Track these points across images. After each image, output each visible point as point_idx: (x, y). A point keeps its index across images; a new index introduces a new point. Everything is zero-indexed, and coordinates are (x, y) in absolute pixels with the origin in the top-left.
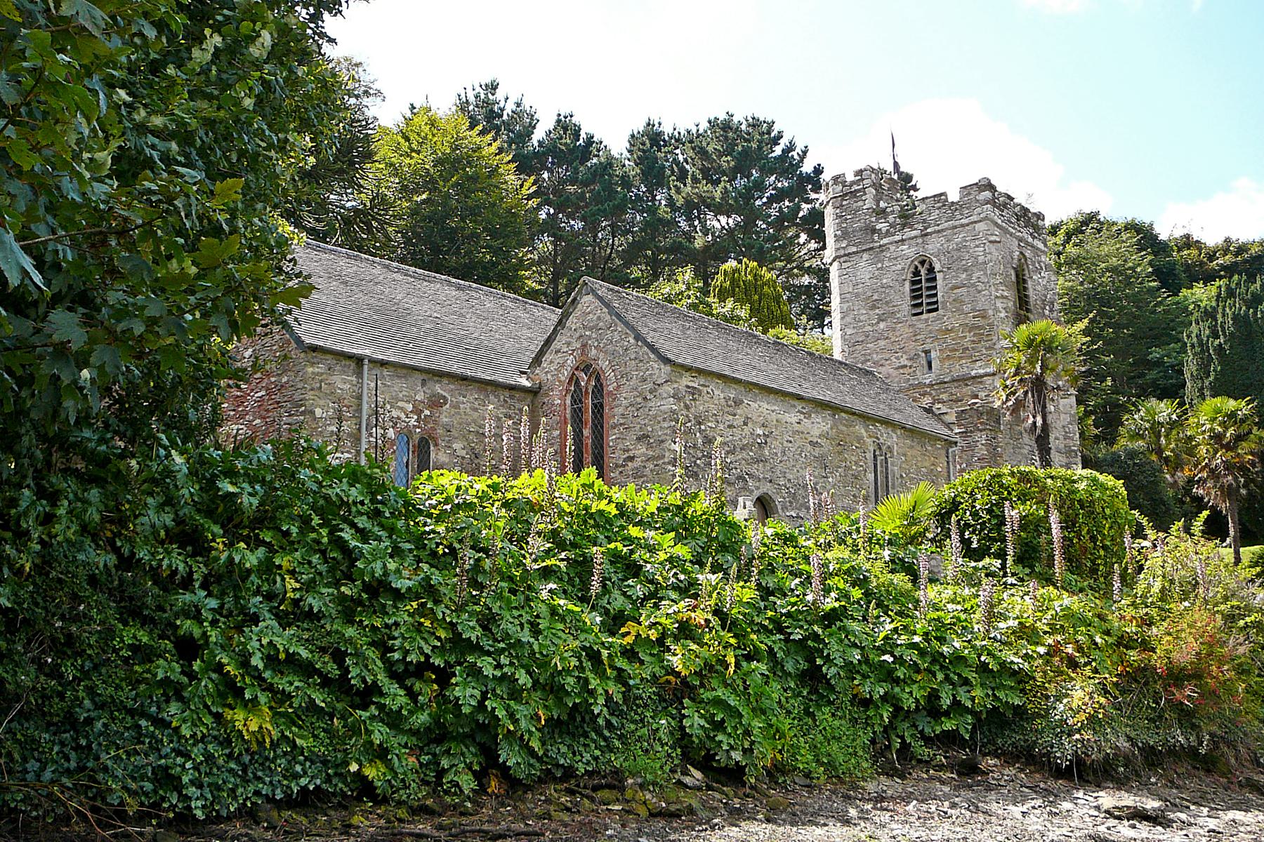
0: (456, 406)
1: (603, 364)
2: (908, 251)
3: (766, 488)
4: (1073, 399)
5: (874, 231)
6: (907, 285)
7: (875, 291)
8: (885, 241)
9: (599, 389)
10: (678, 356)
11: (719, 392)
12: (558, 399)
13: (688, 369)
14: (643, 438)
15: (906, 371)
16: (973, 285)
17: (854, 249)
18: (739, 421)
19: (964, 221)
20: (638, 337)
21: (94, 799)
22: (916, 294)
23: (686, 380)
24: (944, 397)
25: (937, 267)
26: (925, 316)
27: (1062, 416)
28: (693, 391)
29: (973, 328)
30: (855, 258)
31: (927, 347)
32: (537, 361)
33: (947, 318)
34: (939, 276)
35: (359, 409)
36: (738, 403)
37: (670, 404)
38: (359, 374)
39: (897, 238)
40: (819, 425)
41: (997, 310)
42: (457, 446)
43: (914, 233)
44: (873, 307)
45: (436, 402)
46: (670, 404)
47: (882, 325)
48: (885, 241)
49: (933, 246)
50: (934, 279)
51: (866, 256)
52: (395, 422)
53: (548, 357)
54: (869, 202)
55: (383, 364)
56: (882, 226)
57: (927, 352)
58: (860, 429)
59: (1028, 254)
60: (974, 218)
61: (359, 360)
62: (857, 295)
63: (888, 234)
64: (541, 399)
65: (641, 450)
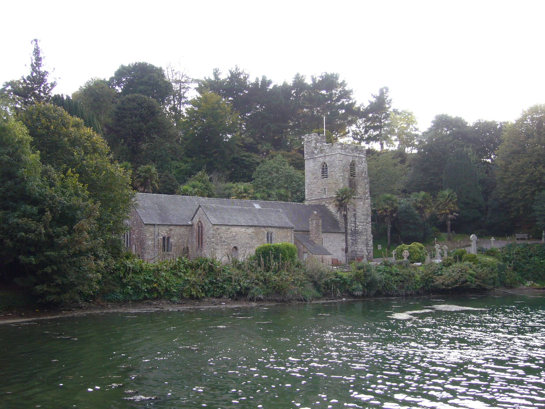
0: (175, 230)
1: (203, 222)
2: (321, 160)
3: (235, 245)
4: (370, 200)
5: (314, 153)
6: (321, 170)
7: (314, 170)
8: (316, 156)
9: (202, 227)
10: (307, 153)
11: (224, 228)
12: (195, 227)
13: (216, 225)
14: (208, 237)
15: (320, 193)
16: (335, 172)
17: (309, 158)
18: (229, 232)
19: (334, 153)
20: (208, 218)
21: (42, 212)
22: (323, 172)
23: (216, 227)
24: (328, 202)
25: (328, 166)
26: (324, 179)
27: (366, 205)
28: (217, 229)
29: (335, 183)
30: (309, 160)
31: (325, 187)
32: (192, 219)
33: (329, 180)
34: (328, 168)
35: (155, 233)
36: (229, 229)
37: (212, 232)
38: (155, 227)
39: (319, 156)
40: (251, 230)
41: (340, 180)
42: (175, 238)
43: (323, 155)
44: (313, 175)
45: (171, 230)
46: (212, 232)
47: (315, 180)
48: (316, 156)
49: (327, 159)
50: (327, 169)
51: (312, 160)
52: (162, 235)
53: (194, 219)
54: (313, 145)
55: (159, 225)
56: (316, 152)
57: (325, 189)
58: (263, 229)
59: (357, 159)
60: (336, 153)
61: (154, 225)
62: (310, 171)
63: (317, 154)
64: (193, 227)
65: (208, 240)
